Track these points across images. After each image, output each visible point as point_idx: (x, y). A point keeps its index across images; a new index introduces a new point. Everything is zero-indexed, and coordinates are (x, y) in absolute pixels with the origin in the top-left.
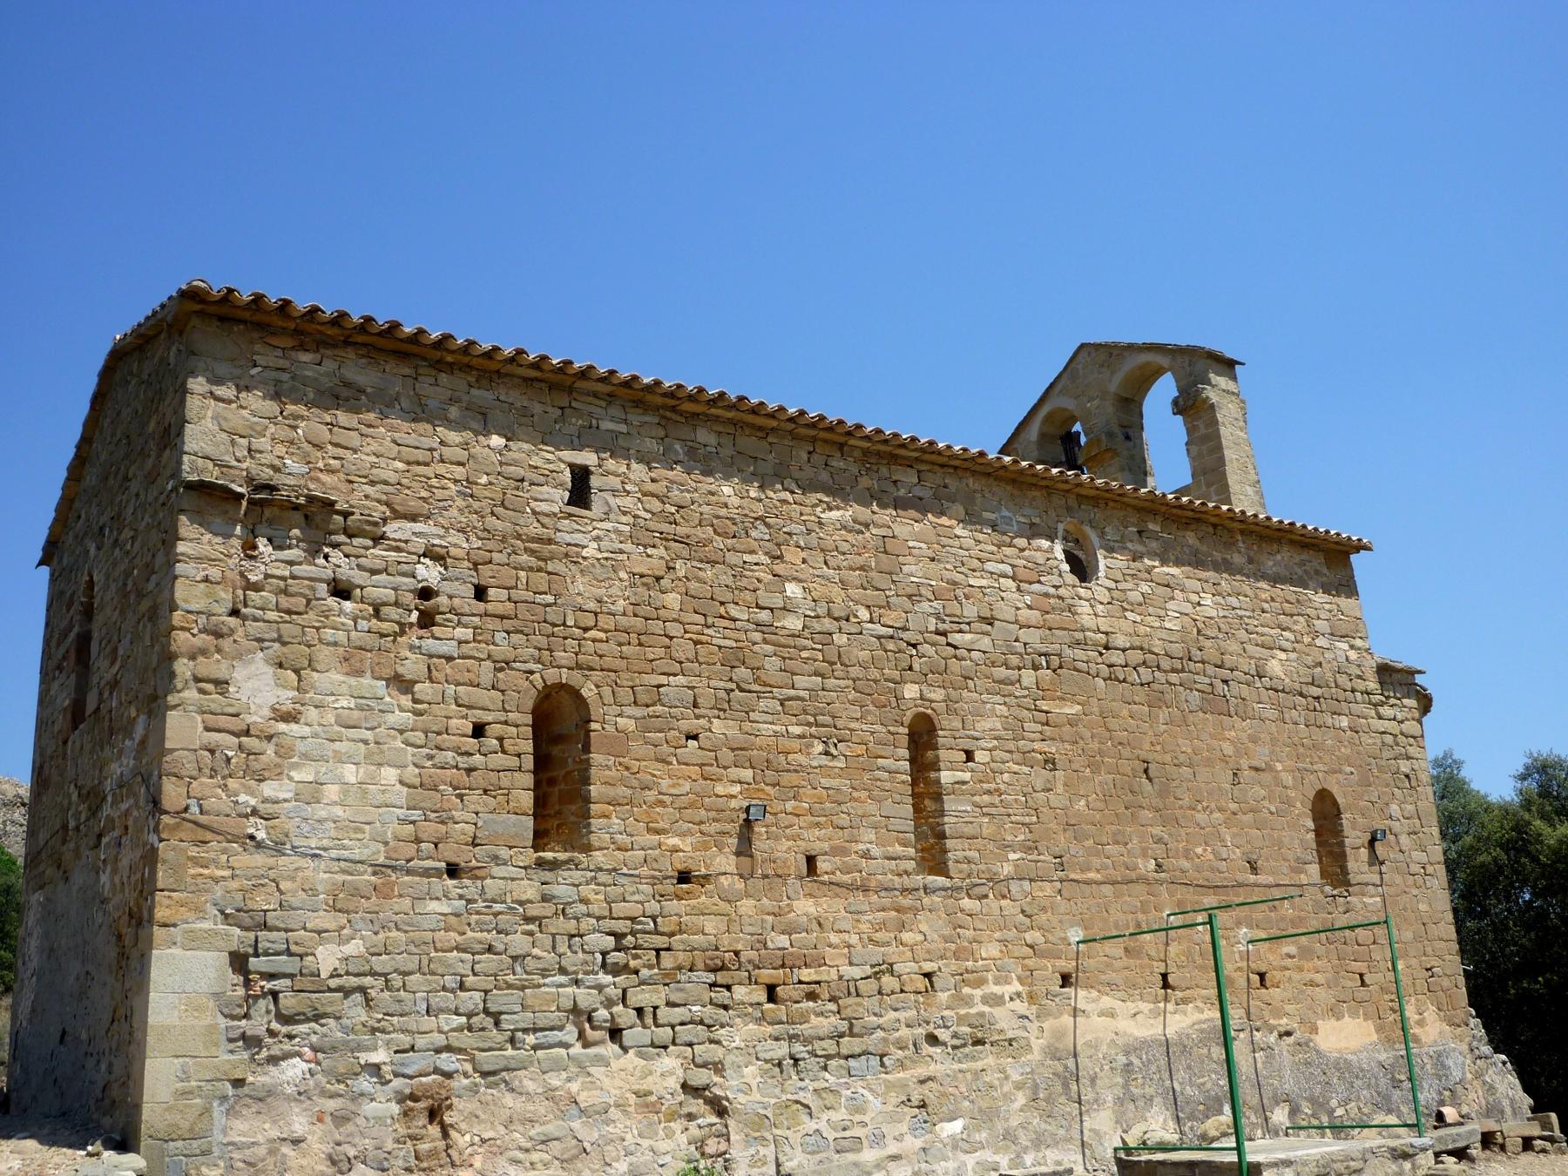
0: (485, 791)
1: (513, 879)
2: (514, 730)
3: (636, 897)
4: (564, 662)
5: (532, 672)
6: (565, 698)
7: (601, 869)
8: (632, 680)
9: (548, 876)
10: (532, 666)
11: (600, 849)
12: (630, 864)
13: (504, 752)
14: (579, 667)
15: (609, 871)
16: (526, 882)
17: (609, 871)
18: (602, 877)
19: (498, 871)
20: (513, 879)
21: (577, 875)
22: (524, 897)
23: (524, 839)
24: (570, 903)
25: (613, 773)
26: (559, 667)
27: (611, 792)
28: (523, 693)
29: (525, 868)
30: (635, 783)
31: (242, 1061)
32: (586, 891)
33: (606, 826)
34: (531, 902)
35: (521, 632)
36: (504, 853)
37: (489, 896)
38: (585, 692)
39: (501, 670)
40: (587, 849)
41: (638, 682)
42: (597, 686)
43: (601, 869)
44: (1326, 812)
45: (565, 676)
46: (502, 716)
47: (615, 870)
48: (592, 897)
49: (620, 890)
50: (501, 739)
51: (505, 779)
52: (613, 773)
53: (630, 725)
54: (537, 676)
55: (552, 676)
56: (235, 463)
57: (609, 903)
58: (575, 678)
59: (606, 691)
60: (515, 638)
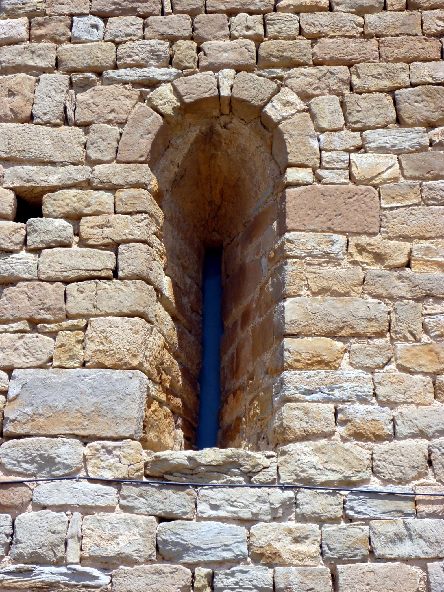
0: (34, 324)
1: (86, 510)
2: (106, 197)
3: (407, 549)
4: (225, 57)
5: (153, 84)
6: (245, 134)
7: (309, 484)
8: (389, 75)
9: (173, 500)
10: (154, 72)
11: (307, 437)
12: (388, 470)
13: (83, 243)
14: (260, 62)
15: (332, 488)
16: (119, 514)
17: (332, 488)
18: (311, 502)
19: (46, 491)
20: (86, 510)
21: (247, 499)
22: (110, 550)
23: (118, 419)
24: (222, 563)
25: (344, 270)
26: (215, 68)
27: (335, 309)
28: (128, 123)
29: (117, 483)
30: (401, 288)
31: (369, 378)
32: (265, 534)
33: (305, 396)
34: (128, 561)
35: (133, 11)
36: (68, 452)
37: (24, 548)
38: (274, 111)
39: (85, 86)
40: (277, 439)
41: (404, 78)
42: (305, 97)
43: (309, 484)
44: (217, 373)
45: (226, 83)
46: (81, 174)
47: (347, 483)
48: (285, 547)
49: (359, 531)
50: (75, 218)
51: (80, 298)
52: (344, 270)
53: (385, 165)
54: (165, 89)
55: (200, 85)
56: (344, 324)
57: (328, 561)
58: (253, 86)
59: (327, 107)
60: (117, 24)
